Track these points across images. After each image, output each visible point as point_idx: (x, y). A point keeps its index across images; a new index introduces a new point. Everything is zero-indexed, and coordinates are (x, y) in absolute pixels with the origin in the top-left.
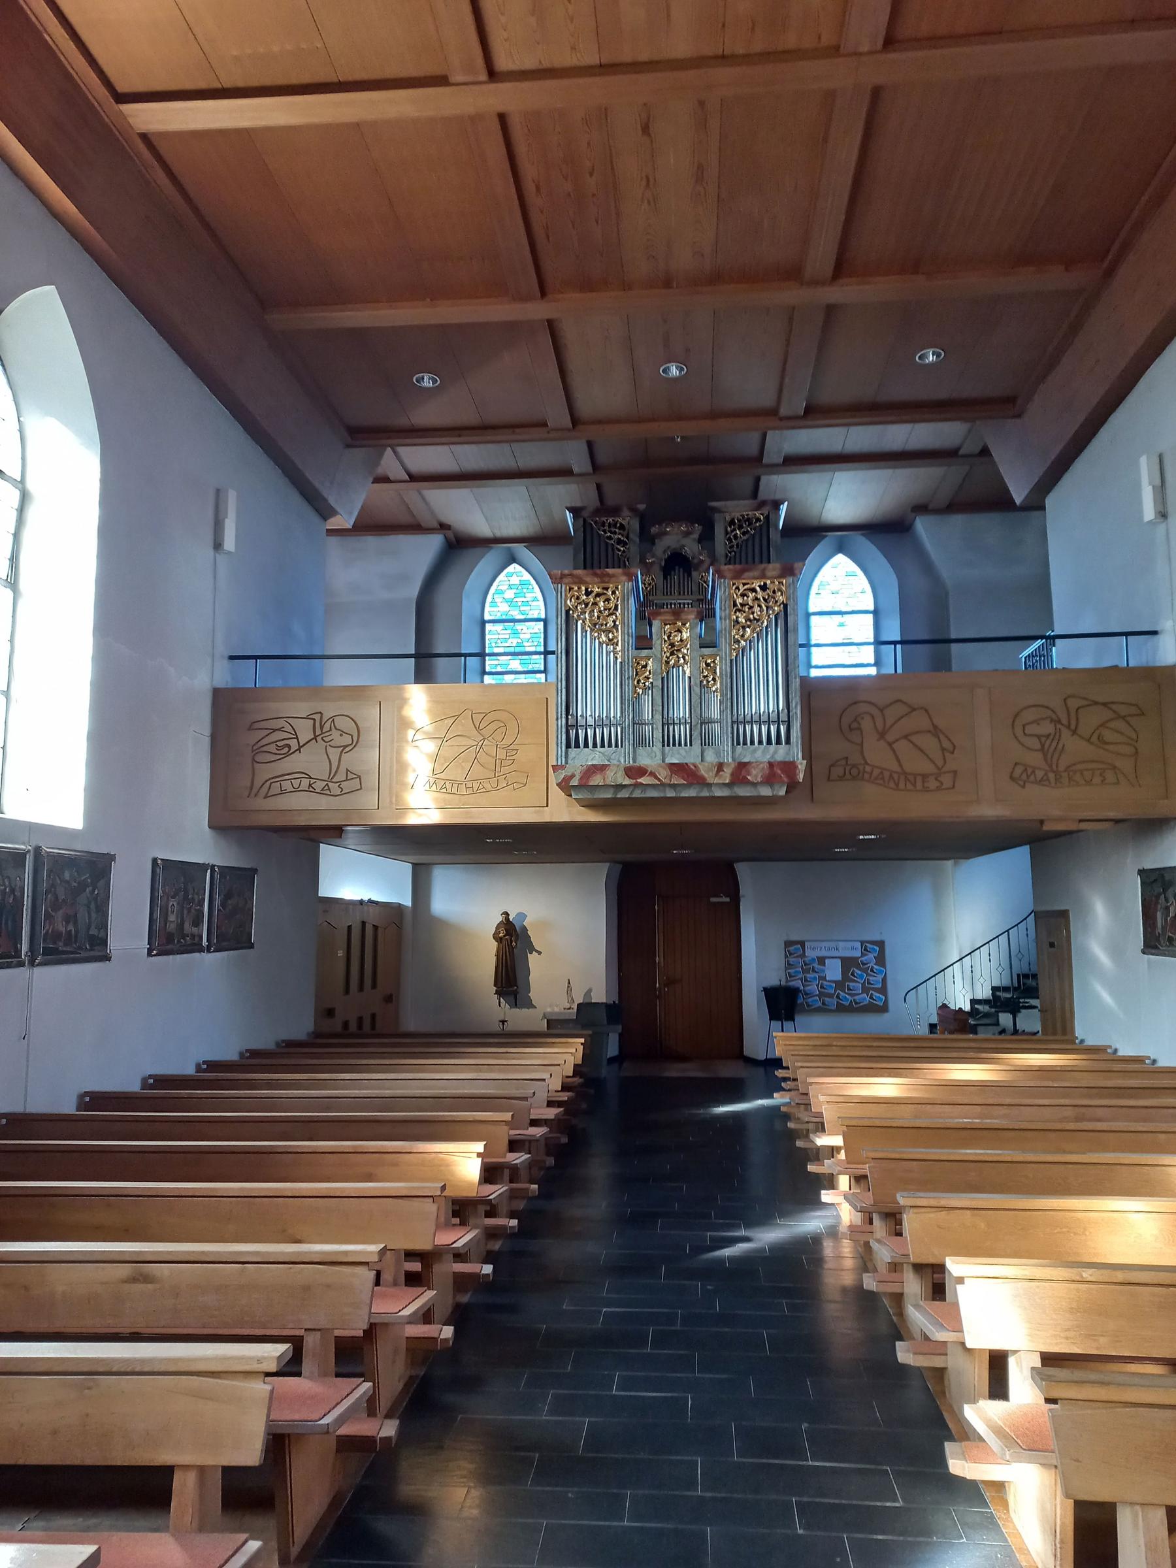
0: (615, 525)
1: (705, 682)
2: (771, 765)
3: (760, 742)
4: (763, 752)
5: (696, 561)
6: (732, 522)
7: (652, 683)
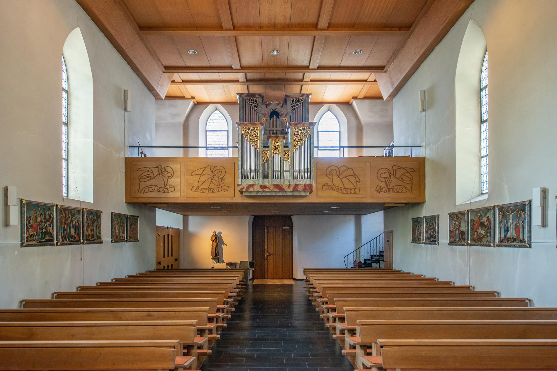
0: (253, 100)
1: (285, 159)
2: (305, 185)
3: (302, 178)
4: (303, 181)
5: (281, 114)
6: (293, 101)
7: (269, 159)
